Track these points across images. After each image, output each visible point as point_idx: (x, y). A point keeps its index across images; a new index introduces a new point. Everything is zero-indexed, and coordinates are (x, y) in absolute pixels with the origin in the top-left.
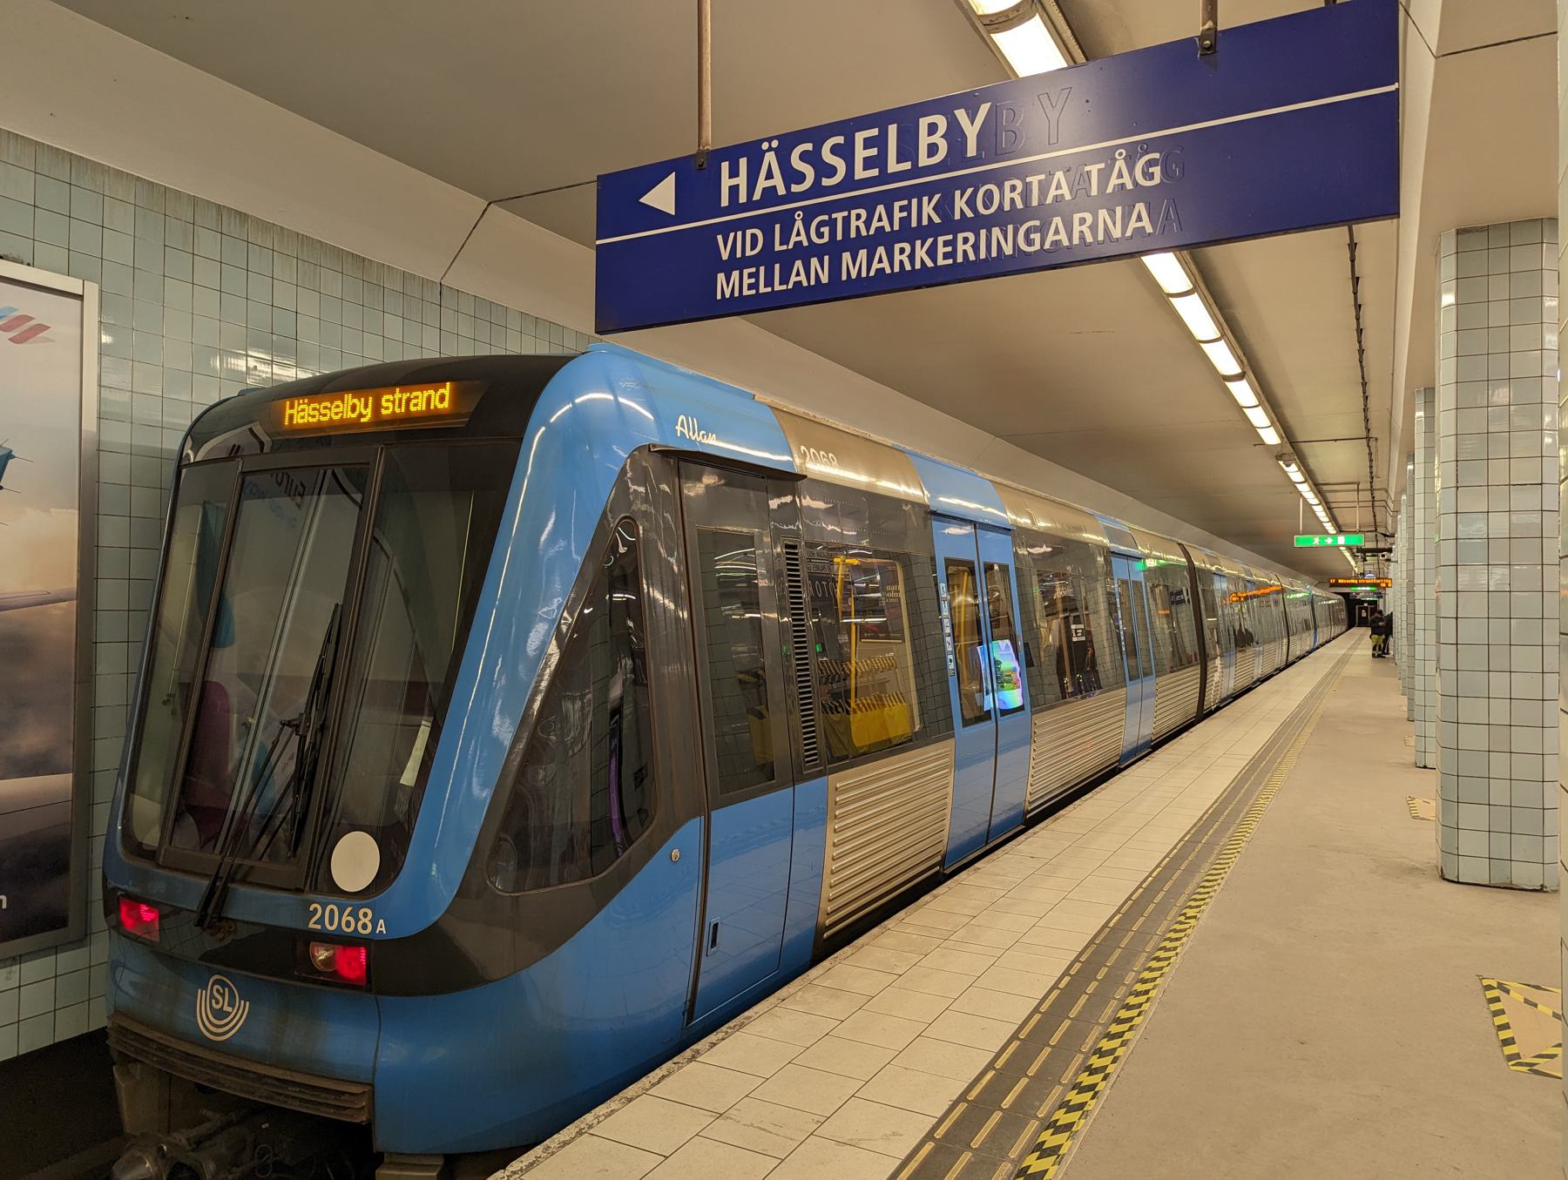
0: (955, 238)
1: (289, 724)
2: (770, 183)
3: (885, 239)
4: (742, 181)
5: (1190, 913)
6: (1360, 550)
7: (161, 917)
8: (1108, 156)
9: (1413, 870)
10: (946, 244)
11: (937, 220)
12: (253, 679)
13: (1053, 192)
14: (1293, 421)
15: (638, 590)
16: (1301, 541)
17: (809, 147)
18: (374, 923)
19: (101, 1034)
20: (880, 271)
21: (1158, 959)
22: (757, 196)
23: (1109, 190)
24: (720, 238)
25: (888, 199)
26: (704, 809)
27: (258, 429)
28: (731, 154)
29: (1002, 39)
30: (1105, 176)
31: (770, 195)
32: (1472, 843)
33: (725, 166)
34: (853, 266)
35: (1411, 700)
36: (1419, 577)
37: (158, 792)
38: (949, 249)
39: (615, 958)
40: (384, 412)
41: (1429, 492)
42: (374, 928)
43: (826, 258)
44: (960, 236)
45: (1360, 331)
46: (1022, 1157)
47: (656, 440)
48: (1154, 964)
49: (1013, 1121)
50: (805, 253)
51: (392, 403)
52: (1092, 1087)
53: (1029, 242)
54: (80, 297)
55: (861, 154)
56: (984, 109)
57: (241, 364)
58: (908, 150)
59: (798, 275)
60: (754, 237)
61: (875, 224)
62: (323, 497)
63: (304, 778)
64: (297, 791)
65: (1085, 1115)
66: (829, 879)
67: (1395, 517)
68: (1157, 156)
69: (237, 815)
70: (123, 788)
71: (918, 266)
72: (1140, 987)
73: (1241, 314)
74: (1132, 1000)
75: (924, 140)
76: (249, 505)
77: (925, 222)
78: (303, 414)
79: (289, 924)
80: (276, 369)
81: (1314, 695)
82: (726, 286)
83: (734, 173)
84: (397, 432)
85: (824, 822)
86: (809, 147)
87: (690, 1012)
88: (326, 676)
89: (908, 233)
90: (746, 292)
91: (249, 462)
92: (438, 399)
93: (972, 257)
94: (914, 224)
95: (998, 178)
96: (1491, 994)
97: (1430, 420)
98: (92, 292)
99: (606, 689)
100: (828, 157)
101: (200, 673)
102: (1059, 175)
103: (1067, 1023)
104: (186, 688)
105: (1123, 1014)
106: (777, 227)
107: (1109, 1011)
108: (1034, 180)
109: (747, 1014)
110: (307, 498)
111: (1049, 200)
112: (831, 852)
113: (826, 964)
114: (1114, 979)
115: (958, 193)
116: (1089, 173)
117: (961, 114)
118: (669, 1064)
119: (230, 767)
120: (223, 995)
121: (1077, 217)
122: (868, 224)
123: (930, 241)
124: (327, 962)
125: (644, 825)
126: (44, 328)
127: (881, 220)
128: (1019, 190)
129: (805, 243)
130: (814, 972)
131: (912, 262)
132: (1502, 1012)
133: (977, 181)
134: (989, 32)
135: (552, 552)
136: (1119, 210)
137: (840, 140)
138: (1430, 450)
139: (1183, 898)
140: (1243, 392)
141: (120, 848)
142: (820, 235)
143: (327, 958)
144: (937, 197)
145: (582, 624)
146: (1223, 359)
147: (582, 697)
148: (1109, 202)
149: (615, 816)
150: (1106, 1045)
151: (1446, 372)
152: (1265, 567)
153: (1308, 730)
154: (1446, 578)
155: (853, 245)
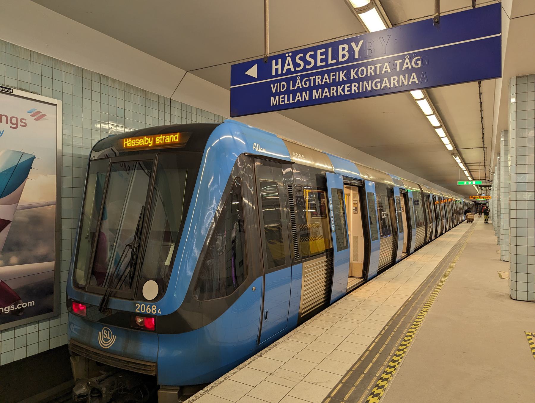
0: (351, 85)
1: (128, 245)
2: (289, 67)
3: (328, 86)
4: (279, 67)
5: (425, 310)
6: (480, 186)
7: (87, 308)
8: (403, 58)
9: (501, 296)
10: (348, 87)
11: (345, 79)
12: (114, 231)
13: (384, 70)
14: (457, 142)
15: (241, 201)
16: (460, 183)
17: (302, 55)
18: (157, 310)
19: (66, 346)
20: (326, 96)
21: (414, 325)
22: (284, 72)
23: (403, 69)
24: (272, 85)
25: (329, 72)
26: (263, 273)
27: (114, 149)
28: (276, 58)
29: (362, 16)
30: (402, 64)
31: (289, 71)
32: (522, 287)
33: (274, 62)
34: (316, 95)
35: (499, 238)
36: (502, 196)
37: (84, 267)
38: (349, 89)
39: (233, 323)
40: (157, 142)
41: (506, 166)
42: (157, 312)
43: (308, 92)
44: (353, 84)
45: (481, 111)
46: (372, 389)
47: (246, 151)
48: (413, 327)
49: (369, 376)
50: (301, 90)
51: (160, 140)
52: (394, 367)
53: (376, 86)
54: (56, 105)
55: (319, 57)
56: (361, 42)
57: (106, 127)
58: (335, 56)
59: (298, 97)
60: (283, 85)
61: (324, 81)
62: (136, 171)
63: (133, 263)
64: (131, 267)
65: (392, 375)
66: (303, 298)
67: (492, 175)
68: (419, 57)
69: (110, 275)
70: (73, 267)
71: (339, 94)
72: (408, 334)
73: (441, 105)
74: (406, 338)
75: (341, 53)
76: (112, 173)
77: (341, 80)
78: (130, 143)
79: (129, 310)
80: (118, 128)
81: (464, 237)
82: (274, 101)
83: (277, 64)
84: (160, 149)
85: (301, 278)
86: (302, 55)
87: (259, 341)
88: (140, 230)
89: (335, 83)
90: (281, 103)
91: (113, 159)
92: (175, 138)
93: (357, 91)
94: (337, 80)
95: (366, 65)
96: (529, 337)
97: (506, 142)
98: (60, 103)
99: (231, 234)
100: (308, 58)
101: (98, 229)
102: (386, 64)
103: (385, 346)
104: (93, 234)
105: (403, 343)
106: (291, 82)
107: (398, 342)
108: (378, 66)
109: (277, 341)
110: (131, 171)
111: (383, 73)
112: (303, 288)
113: (302, 325)
114: (400, 331)
115: (352, 70)
116: (396, 63)
117: (353, 44)
118: (253, 357)
119: (107, 259)
120: (107, 334)
121: (392, 78)
122: (322, 80)
123: (343, 86)
124: (141, 323)
125: (243, 279)
126: (44, 115)
127: (326, 79)
128: (373, 69)
129: (301, 87)
130: (298, 328)
131: (337, 93)
132: (533, 343)
133: (358, 66)
134: (358, 13)
135: (212, 189)
136: (407, 75)
137: (312, 53)
138: (506, 152)
139: (422, 305)
140: (441, 132)
141: (72, 286)
142: (306, 84)
143: (141, 322)
144: (345, 71)
145: (223, 212)
146: (434, 121)
147: (222, 236)
148: (403, 73)
149: (233, 276)
150: (398, 353)
151: (512, 126)
152: (446, 192)
153: (464, 247)
154: (513, 196)
155: (317, 88)
